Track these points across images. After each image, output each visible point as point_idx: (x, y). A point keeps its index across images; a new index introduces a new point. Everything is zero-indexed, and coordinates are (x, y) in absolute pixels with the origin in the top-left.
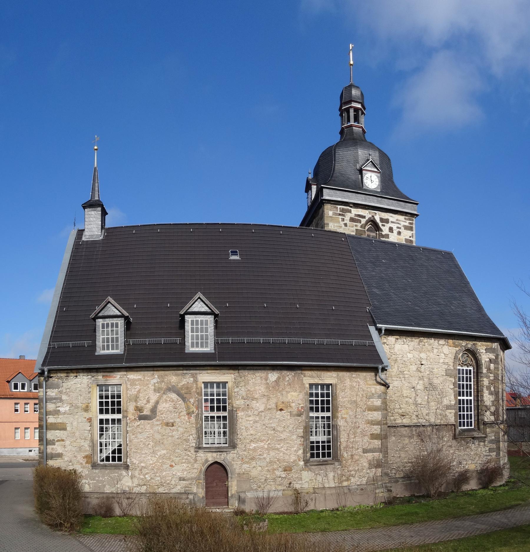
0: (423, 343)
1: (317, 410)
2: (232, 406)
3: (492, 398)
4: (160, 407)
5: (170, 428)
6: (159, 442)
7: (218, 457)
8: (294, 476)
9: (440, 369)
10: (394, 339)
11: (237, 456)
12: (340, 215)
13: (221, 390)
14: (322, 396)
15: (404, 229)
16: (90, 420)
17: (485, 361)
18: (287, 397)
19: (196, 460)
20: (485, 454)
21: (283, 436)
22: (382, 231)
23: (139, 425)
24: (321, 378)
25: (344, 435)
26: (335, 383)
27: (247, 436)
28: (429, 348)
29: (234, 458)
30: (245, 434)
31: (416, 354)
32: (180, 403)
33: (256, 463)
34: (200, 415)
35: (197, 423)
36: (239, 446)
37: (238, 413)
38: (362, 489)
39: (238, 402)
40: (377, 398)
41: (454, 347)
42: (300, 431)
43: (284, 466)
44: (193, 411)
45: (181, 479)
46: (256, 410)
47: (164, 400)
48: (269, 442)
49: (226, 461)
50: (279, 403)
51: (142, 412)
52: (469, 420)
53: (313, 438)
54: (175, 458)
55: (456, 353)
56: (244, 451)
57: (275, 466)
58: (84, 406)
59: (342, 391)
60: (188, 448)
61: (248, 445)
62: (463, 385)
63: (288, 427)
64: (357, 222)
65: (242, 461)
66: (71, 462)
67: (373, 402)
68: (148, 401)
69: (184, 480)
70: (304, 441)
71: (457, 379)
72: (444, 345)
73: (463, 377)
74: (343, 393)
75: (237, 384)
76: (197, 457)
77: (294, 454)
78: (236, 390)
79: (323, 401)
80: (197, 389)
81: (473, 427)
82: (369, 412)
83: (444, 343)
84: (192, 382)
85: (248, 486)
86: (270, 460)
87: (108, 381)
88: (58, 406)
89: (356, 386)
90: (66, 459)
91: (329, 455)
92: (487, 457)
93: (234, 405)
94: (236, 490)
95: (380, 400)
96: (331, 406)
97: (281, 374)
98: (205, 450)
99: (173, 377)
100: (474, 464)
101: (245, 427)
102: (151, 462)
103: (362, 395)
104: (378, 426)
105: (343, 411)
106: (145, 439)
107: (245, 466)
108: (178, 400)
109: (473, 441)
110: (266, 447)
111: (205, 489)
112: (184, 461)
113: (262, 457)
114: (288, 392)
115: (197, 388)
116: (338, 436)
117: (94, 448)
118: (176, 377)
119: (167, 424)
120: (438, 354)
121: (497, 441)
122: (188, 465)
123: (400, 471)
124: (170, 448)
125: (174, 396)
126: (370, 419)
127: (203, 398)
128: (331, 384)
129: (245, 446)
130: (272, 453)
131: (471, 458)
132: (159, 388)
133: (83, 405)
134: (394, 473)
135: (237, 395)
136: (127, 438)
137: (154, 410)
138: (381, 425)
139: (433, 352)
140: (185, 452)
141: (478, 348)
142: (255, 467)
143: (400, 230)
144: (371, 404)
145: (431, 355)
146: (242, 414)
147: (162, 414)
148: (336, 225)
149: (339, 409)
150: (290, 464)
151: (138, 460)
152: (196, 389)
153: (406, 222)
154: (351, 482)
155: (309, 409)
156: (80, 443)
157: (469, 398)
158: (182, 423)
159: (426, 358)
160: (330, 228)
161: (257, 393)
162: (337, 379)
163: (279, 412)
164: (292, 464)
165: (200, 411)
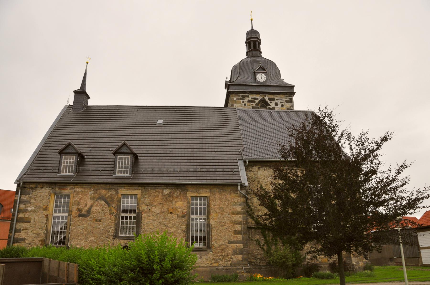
2: (139, 210)
4: (93, 209)
5: (98, 223)
6: (90, 232)
7: (128, 243)
12: (241, 99)
14: (200, 205)
15: (286, 103)
16: (47, 216)
19: (113, 244)
21: (172, 230)
22: (270, 105)
23: (78, 220)
24: (199, 192)
26: (208, 196)
27: (147, 230)
30: (146, 228)
32: (106, 207)
34: (118, 215)
35: (115, 220)
38: (227, 269)
40: (238, 205)
44: (114, 213)
46: (155, 213)
47: (96, 205)
50: (170, 209)
51: (81, 212)
54: (99, 243)
58: (44, 207)
59: (214, 201)
63: (175, 224)
64: (253, 102)
66: (30, 244)
67: (235, 208)
68: (86, 205)
70: (186, 234)
75: (143, 196)
78: (142, 200)
82: (233, 215)
87: (62, 192)
88: (27, 206)
89: (224, 197)
90: (27, 242)
93: (140, 209)
95: (241, 207)
102: (84, 245)
103: (228, 204)
104: (239, 225)
105: (214, 214)
106: (82, 229)
114: (176, 202)
115: (117, 198)
117: (48, 235)
118: (105, 191)
119: (97, 220)
124: (97, 236)
125: (103, 202)
126: (233, 220)
132: (94, 197)
133: (44, 206)
134: (259, 262)
136: (69, 229)
137: (89, 211)
140: (107, 239)
143: (283, 104)
146: (145, 215)
147: (94, 214)
148: (238, 105)
149: (211, 213)
151: (75, 243)
152: (117, 198)
154: (219, 264)
156: (39, 231)
158: (106, 220)
163: (170, 214)
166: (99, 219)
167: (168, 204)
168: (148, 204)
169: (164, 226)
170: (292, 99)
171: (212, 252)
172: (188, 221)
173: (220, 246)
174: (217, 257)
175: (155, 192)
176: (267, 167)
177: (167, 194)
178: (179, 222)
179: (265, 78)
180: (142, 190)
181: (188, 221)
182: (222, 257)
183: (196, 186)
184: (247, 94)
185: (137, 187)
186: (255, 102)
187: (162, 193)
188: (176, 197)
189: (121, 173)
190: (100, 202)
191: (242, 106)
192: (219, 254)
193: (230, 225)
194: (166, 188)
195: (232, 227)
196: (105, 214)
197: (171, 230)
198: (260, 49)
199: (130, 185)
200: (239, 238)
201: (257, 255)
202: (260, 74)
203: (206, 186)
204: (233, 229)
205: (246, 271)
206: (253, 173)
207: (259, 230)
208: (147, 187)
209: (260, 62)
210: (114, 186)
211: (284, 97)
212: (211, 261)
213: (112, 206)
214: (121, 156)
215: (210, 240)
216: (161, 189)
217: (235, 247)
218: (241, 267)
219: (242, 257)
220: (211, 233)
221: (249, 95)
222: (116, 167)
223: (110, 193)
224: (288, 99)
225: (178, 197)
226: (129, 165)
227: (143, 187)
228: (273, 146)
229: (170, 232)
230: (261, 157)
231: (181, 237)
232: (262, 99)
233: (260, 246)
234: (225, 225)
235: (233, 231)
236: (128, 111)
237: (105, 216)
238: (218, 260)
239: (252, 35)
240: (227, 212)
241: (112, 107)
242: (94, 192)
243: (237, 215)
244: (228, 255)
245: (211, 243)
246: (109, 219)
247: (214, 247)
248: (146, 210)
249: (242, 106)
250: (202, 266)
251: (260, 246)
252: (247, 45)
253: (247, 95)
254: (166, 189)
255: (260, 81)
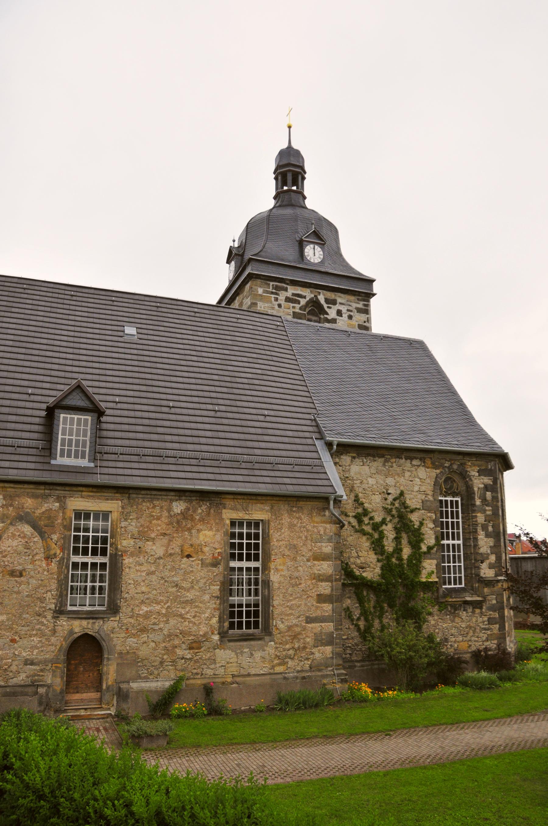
0: (390, 464)
1: (241, 559)
2: (116, 549)
3: (491, 542)
7: (90, 626)
8: (204, 656)
9: (414, 501)
10: (350, 458)
11: (120, 625)
12: (272, 293)
13: (101, 523)
15: (357, 312)
17: (479, 488)
18: (198, 538)
19: (54, 632)
20: (483, 627)
21: (190, 595)
22: (327, 314)
24: (248, 511)
25: (279, 596)
26: (267, 519)
27: (136, 595)
28: (399, 470)
29: (114, 628)
30: (132, 591)
31: (380, 479)
32: (35, 539)
33: (148, 637)
34: (65, 561)
35: (59, 573)
36: (124, 609)
37: (124, 560)
38: (304, 678)
39: (126, 543)
41: (433, 468)
42: (216, 589)
43: (189, 642)
44: (55, 554)
45: (29, 662)
46: (152, 555)
47: (10, 534)
48: (169, 604)
49: (101, 633)
50: (186, 546)
52: (457, 575)
53: (235, 599)
54: (20, 628)
55: (436, 477)
56: (130, 618)
57: (176, 642)
60: (43, 611)
61: (137, 609)
62: (447, 523)
63: (198, 582)
64: (295, 303)
65: (126, 633)
69: (32, 663)
70: (220, 604)
71: (439, 515)
72: (418, 466)
73: (447, 512)
74: (279, 534)
75: (125, 516)
76: (56, 627)
77: (205, 623)
78: (123, 524)
79: (249, 545)
80: (64, 521)
81: (463, 586)
82: (316, 562)
83: (419, 463)
84: (57, 509)
85: (134, 672)
86: (169, 632)
89: (297, 523)
91: (256, 626)
92: (486, 632)
93: (119, 546)
94: (115, 678)
95: (331, 544)
96: (260, 552)
97: (190, 504)
98: (70, 616)
99: (29, 499)
100: (466, 642)
101: (134, 581)
103: (306, 537)
104: (327, 583)
105: (278, 560)
107: (131, 641)
108: (32, 535)
109: (464, 608)
110: (164, 611)
111: (65, 678)
112: (34, 632)
113: (156, 627)
114: (199, 531)
115: (64, 518)
116: (271, 597)
118: (33, 500)
119: (12, 573)
120: (410, 479)
121: (500, 608)
122: (40, 639)
123: (358, 651)
124: (14, 611)
125: (27, 529)
126: (316, 572)
127: (73, 534)
128: (262, 520)
129: (132, 609)
130: (172, 622)
131: (462, 633)
134: (350, 654)
135: (124, 532)
138: (332, 581)
139: (404, 476)
140: (38, 618)
141: (468, 470)
142: (145, 642)
143: (352, 314)
144: (318, 551)
145: (402, 479)
146: (131, 560)
148: (266, 305)
149: (273, 557)
150: (198, 638)
152: (62, 520)
153: (359, 303)
154: (289, 666)
155: (229, 555)
157: (456, 542)
158: (36, 572)
159: (394, 484)
160: (259, 308)
161: (155, 530)
162: (270, 514)
163: (185, 559)
164: (202, 638)
165: (65, 554)
166: (18, 570)
167: (182, 536)
168: (136, 535)
169: (173, 587)
170: (368, 305)
171: (273, 641)
172: (224, 574)
173: (290, 628)
174: (284, 653)
175: (153, 508)
176: (368, 456)
177: (179, 512)
178: (205, 578)
179: (322, 257)
180: (121, 500)
181: (224, 574)
182: (294, 652)
183: (242, 497)
184: (285, 283)
185: (110, 494)
186: (299, 303)
187: (169, 510)
188: (200, 521)
189: (69, 456)
190: (19, 527)
191: (273, 308)
192: (287, 646)
193: (309, 582)
194: (177, 498)
195: (314, 587)
196: (33, 557)
197: (188, 594)
198: (303, 189)
199: (94, 490)
200: (327, 611)
201: (345, 639)
202: (312, 246)
203: (264, 498)
204: (315, 591)
205: (340, 680)
206: (341, 468)
207: (351, 588)
208: (134, 496)
209: (313, 222)
210: (57, 490)
211: (354, 300)
212: (272, 662)
213: (52, 539)
214: (69, 416)
215: (271, 617)
216: (166, 501)
217: (319, 629)
218: (330, 671)
219: (331, 650)
220: (273, 600)
221: (289, 287)
222: (57, 442)
223: (46, 507)
224: (360, 305)
225: (203, 520)
226: (88, 439)
227: (125, 495)
228: (371, 412)
229: (187, 600)
230: (358, 436)
231: (209, 611)
232: (312, 298)
233: (352, 620)
234: (300, 584)
235: (314, 595)
236: (50, 294)
237: (33, 562)
238: (285, 658)
239: (292, 159)
240: (303, 556)
241: (9, 280)
242: (4, 503)
243: (323, 561)
244: (305, 648)
245: (273, 623)
246: (44, 570)
247: (278, 632)
248: (132, 549)
249: (273, 308)
250: (253, 672)
251: (352, 620)
252: (280, 178)
253: (285, 286)
254: (177, 500)
255: (312, 261)
